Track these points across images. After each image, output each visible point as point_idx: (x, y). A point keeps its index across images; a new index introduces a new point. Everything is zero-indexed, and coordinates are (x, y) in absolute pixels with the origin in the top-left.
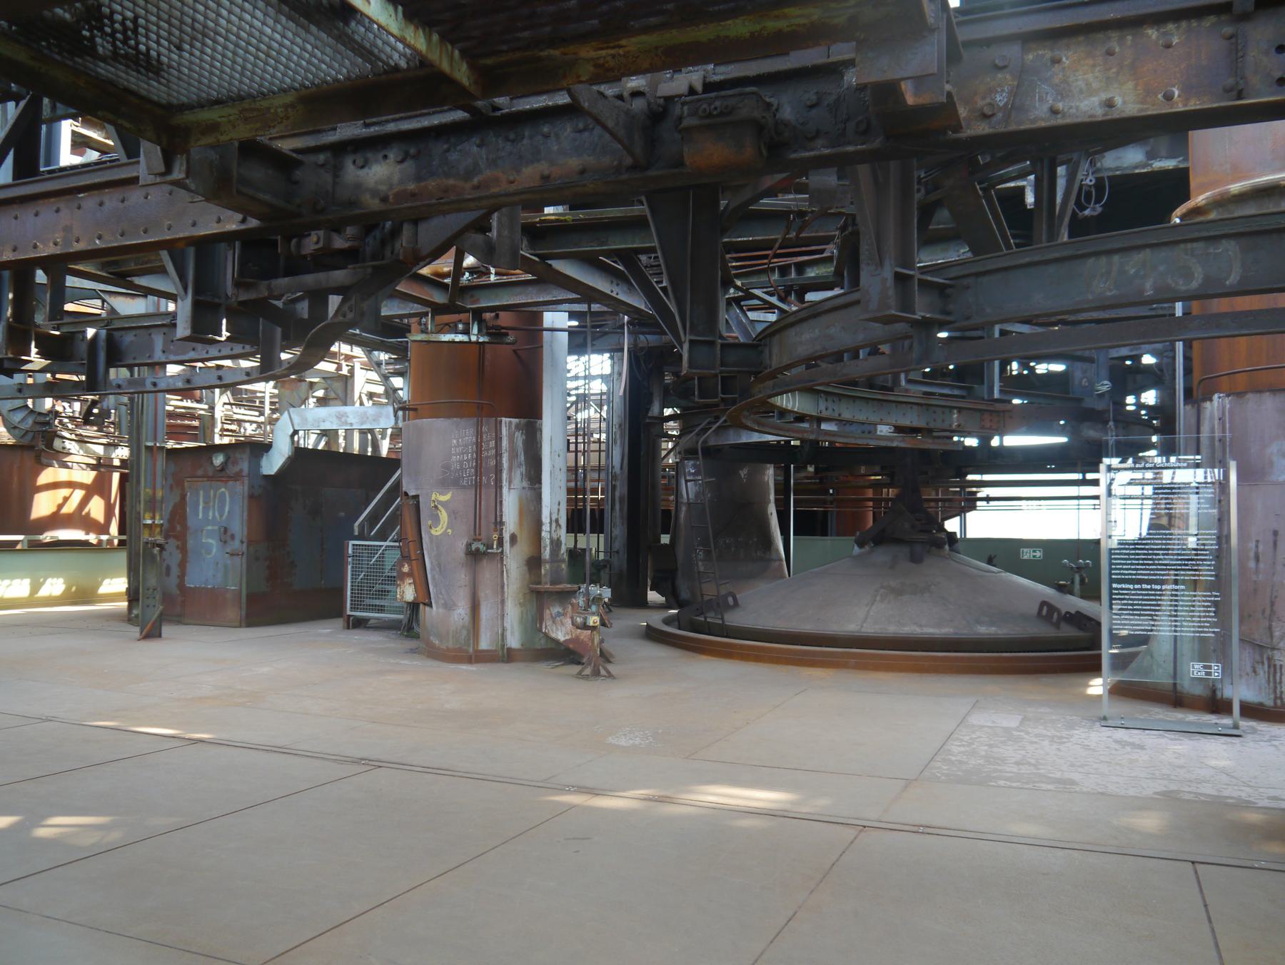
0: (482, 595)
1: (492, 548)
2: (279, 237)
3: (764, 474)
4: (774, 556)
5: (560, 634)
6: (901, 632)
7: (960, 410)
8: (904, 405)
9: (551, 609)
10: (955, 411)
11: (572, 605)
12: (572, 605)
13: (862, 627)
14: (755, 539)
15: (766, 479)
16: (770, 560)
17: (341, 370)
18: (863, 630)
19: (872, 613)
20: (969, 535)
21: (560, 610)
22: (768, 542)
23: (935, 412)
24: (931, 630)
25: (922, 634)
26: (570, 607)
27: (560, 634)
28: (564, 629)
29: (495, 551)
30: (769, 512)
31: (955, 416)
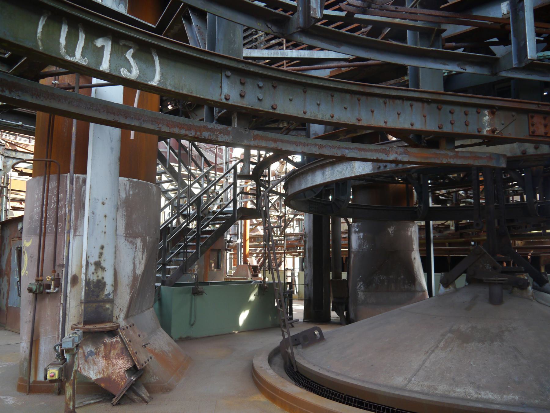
0: (42, 330)
1: (50, 288)
2: (431, 205)
3: (407, 230)
4: (418, 288)
5: (91, 372)
6: (452, 394)
7: (493, 110)
8: (398, 102)
9: (84, 348)
10: (486, 112)
11: (105, 344)
12: (105, 344)
13: (410, 381)
14: (402, 277)
15: (409, 234)
16: (415, 291)
17: (420, 229)
18: (410, 387)
19: (427, 364)
20: (293, 300)
21: (93, 349)
22: (412, 278)
23: (451, 113)
24: (490, 396)
25: (477, 400)
26: (103, 346)
27: (91, 372)
28: (96, 368)
29: (51, 291)
30: (413, 257)
31: (486, 118)
